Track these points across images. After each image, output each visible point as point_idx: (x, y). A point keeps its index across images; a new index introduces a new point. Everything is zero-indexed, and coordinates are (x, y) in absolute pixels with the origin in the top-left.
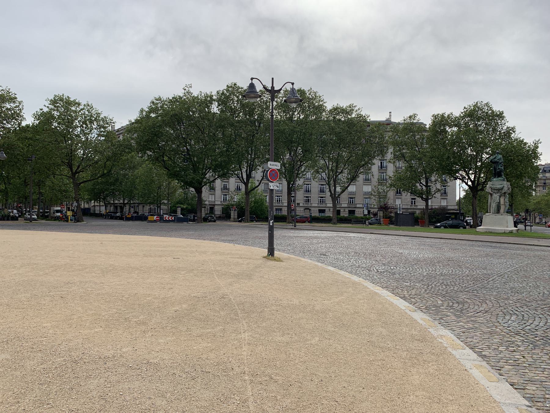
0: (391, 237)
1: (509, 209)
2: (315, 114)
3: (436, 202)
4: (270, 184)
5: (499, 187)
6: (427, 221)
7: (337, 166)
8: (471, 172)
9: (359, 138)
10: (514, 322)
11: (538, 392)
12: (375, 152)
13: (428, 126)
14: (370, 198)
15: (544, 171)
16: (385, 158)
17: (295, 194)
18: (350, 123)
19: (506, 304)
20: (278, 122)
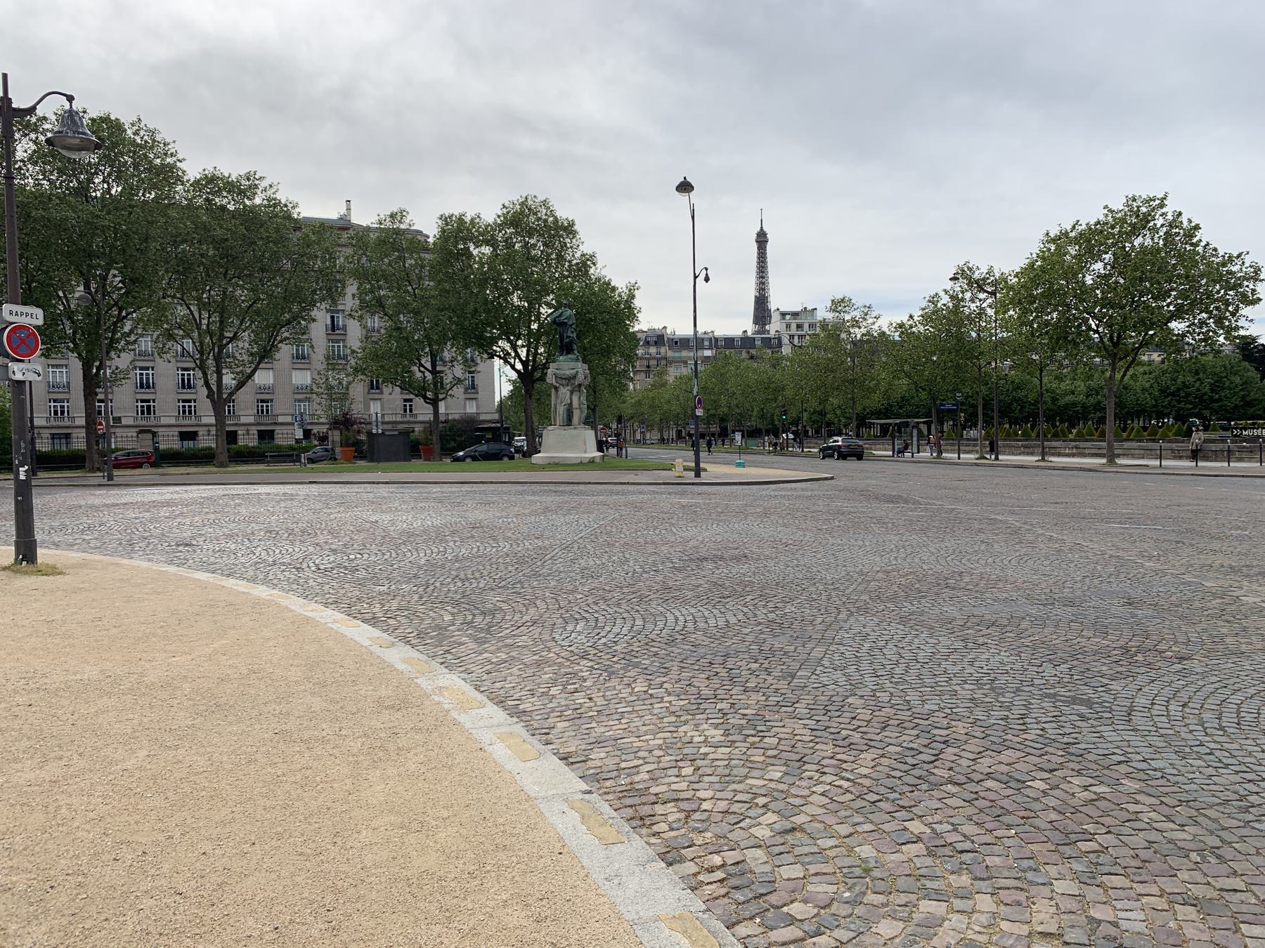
0: (355, 488)
1: (587, 418)
2: (154, 187)
3: (455, 407)
4: (14, 366)
5: (569, 373)
6: (437, 448)
7: (221, 322)
8: (519, 343)
9: (275, 257)
10: (579, 635)
11: (607, 761)
12: (314, 292)
13: (431, 240)
14: (308, 399)
15: (647, 343)
16: (340, 307)
17: (106, 394)
18: (250, 218)
19: (570, 602)
20: (41, 198)
